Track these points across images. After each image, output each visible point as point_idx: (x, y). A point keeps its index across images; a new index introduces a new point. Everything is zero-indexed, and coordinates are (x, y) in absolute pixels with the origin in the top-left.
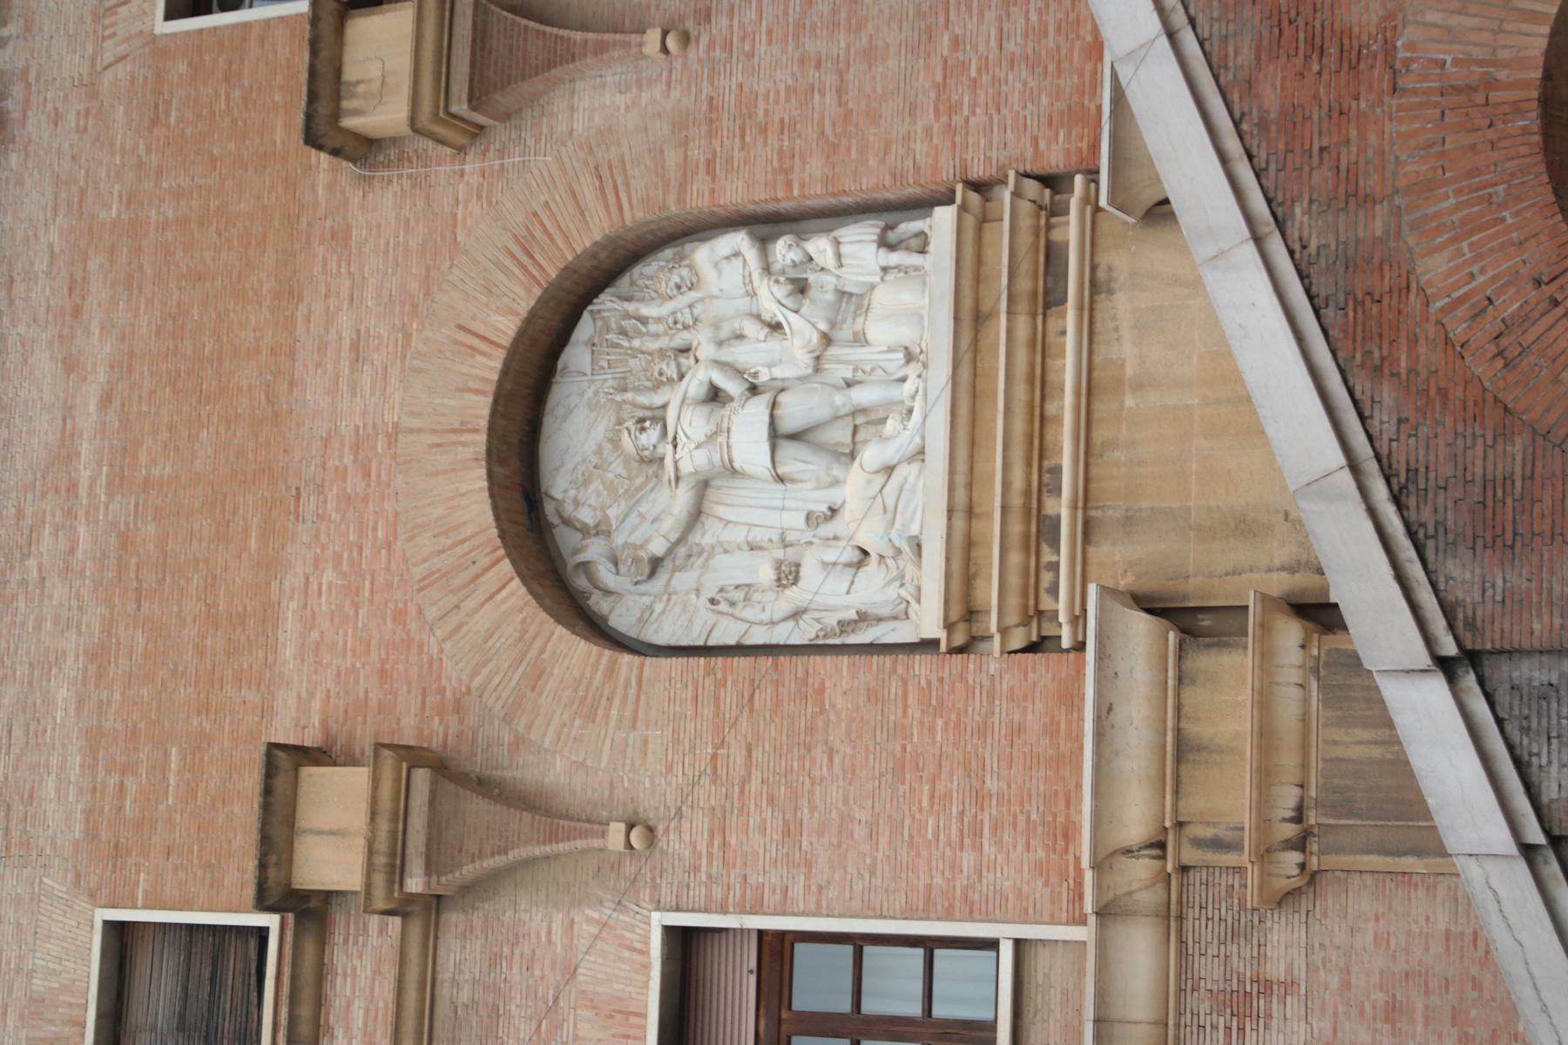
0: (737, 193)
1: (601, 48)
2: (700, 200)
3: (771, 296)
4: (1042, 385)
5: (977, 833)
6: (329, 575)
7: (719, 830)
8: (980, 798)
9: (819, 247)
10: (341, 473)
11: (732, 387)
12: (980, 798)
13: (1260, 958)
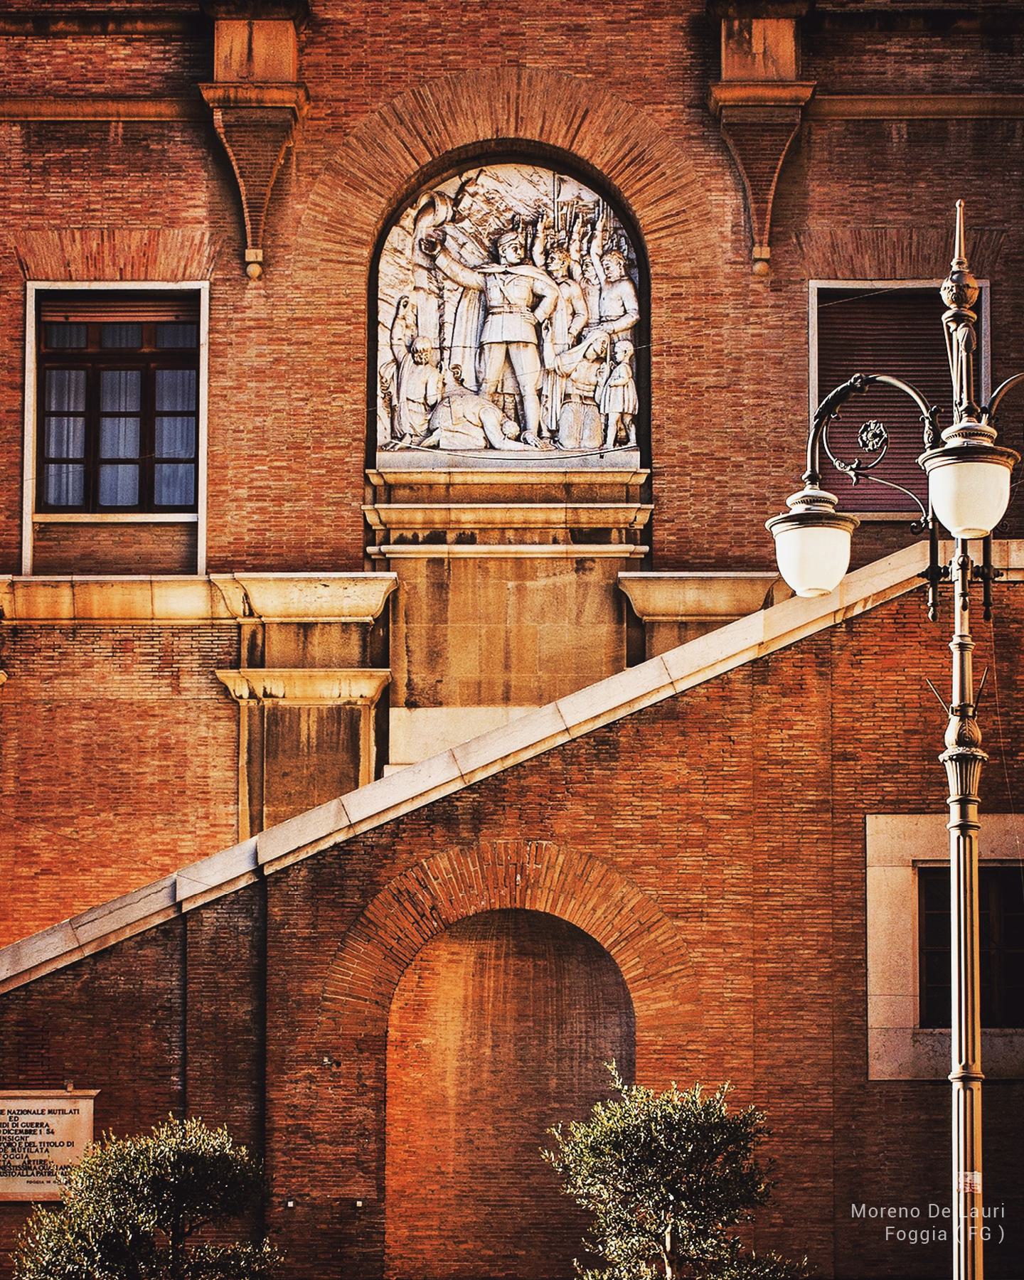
0: (659, 315)
1: (761, 214)
2: (659, 289)
3: (596, 339)
4: (522, 533)
5: (260, 498)
6: (426, 18)
7: (260, 325)
8: (279, 500)
9: (624, 373)
10: (492, 22)
11: (545, 308)
12: (279, 500)
13: (191, 673)
